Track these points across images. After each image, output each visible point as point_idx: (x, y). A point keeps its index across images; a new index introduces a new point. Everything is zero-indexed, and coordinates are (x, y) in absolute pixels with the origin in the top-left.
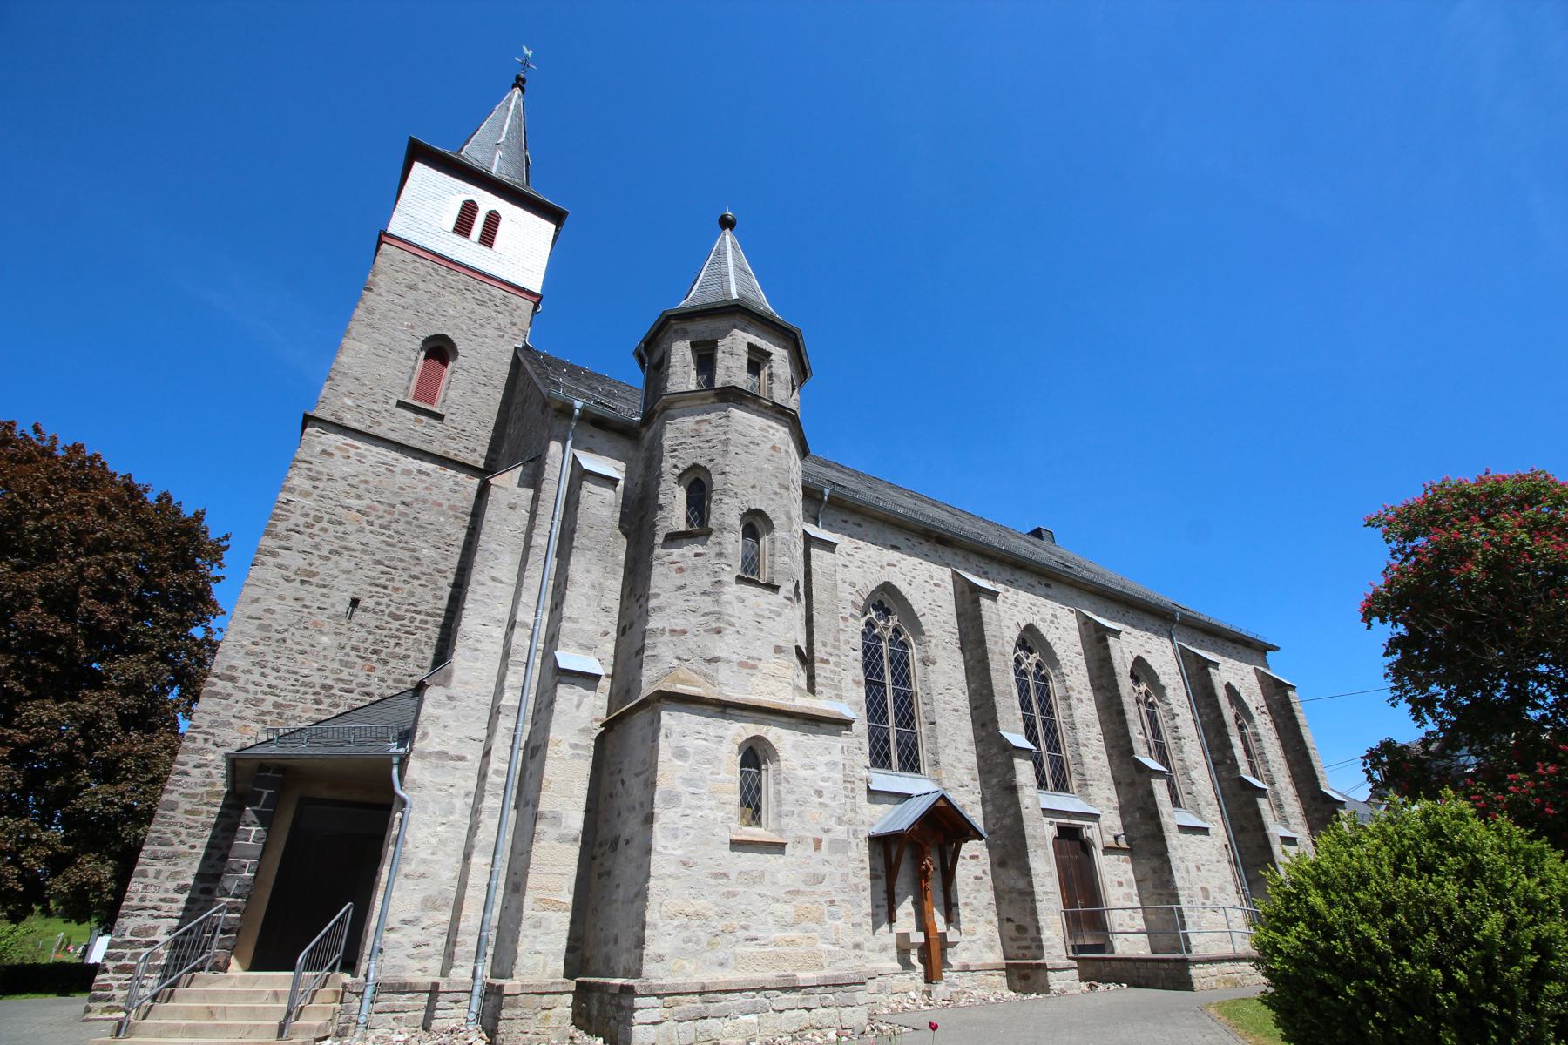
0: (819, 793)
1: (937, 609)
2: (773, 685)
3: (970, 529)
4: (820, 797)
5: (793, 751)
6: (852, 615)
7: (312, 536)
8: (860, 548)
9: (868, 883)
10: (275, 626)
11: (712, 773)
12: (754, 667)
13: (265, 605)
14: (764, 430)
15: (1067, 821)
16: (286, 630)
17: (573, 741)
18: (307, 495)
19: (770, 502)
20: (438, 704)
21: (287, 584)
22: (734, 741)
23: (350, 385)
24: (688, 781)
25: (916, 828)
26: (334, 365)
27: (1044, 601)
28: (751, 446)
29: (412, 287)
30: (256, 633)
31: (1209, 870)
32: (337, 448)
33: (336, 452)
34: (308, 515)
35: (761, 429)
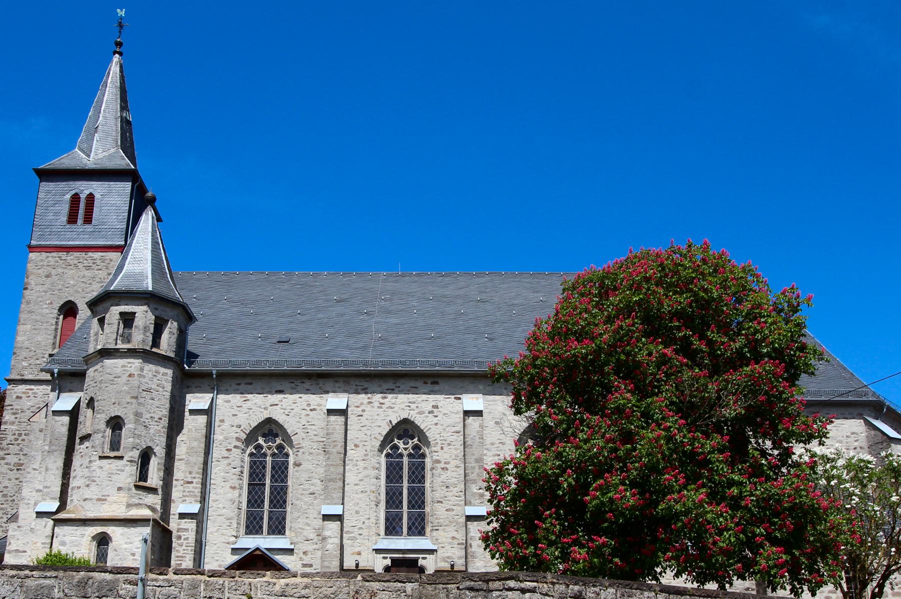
0: (133, 555)
1: (309, 427)
2: (114, 507)
4: (134, 556)
5: (121, 537)
6: (235, 447)
8: (248, 400)
10: (9, 494)
11: (77, 550)
15: (401, 556)
16: (14, 495)
17: (43, 542)
18: (13, 423)
19: (124, 409)
20: (14, 530)
21: (12, 472)
23: (24, 354)
26: (15, 345)
27: (424, 397)
28: (116, 379)
29: (48, 276)
32: (23, 393)
33: (23, 395)
34: (15, 434)
35: (123, 366)
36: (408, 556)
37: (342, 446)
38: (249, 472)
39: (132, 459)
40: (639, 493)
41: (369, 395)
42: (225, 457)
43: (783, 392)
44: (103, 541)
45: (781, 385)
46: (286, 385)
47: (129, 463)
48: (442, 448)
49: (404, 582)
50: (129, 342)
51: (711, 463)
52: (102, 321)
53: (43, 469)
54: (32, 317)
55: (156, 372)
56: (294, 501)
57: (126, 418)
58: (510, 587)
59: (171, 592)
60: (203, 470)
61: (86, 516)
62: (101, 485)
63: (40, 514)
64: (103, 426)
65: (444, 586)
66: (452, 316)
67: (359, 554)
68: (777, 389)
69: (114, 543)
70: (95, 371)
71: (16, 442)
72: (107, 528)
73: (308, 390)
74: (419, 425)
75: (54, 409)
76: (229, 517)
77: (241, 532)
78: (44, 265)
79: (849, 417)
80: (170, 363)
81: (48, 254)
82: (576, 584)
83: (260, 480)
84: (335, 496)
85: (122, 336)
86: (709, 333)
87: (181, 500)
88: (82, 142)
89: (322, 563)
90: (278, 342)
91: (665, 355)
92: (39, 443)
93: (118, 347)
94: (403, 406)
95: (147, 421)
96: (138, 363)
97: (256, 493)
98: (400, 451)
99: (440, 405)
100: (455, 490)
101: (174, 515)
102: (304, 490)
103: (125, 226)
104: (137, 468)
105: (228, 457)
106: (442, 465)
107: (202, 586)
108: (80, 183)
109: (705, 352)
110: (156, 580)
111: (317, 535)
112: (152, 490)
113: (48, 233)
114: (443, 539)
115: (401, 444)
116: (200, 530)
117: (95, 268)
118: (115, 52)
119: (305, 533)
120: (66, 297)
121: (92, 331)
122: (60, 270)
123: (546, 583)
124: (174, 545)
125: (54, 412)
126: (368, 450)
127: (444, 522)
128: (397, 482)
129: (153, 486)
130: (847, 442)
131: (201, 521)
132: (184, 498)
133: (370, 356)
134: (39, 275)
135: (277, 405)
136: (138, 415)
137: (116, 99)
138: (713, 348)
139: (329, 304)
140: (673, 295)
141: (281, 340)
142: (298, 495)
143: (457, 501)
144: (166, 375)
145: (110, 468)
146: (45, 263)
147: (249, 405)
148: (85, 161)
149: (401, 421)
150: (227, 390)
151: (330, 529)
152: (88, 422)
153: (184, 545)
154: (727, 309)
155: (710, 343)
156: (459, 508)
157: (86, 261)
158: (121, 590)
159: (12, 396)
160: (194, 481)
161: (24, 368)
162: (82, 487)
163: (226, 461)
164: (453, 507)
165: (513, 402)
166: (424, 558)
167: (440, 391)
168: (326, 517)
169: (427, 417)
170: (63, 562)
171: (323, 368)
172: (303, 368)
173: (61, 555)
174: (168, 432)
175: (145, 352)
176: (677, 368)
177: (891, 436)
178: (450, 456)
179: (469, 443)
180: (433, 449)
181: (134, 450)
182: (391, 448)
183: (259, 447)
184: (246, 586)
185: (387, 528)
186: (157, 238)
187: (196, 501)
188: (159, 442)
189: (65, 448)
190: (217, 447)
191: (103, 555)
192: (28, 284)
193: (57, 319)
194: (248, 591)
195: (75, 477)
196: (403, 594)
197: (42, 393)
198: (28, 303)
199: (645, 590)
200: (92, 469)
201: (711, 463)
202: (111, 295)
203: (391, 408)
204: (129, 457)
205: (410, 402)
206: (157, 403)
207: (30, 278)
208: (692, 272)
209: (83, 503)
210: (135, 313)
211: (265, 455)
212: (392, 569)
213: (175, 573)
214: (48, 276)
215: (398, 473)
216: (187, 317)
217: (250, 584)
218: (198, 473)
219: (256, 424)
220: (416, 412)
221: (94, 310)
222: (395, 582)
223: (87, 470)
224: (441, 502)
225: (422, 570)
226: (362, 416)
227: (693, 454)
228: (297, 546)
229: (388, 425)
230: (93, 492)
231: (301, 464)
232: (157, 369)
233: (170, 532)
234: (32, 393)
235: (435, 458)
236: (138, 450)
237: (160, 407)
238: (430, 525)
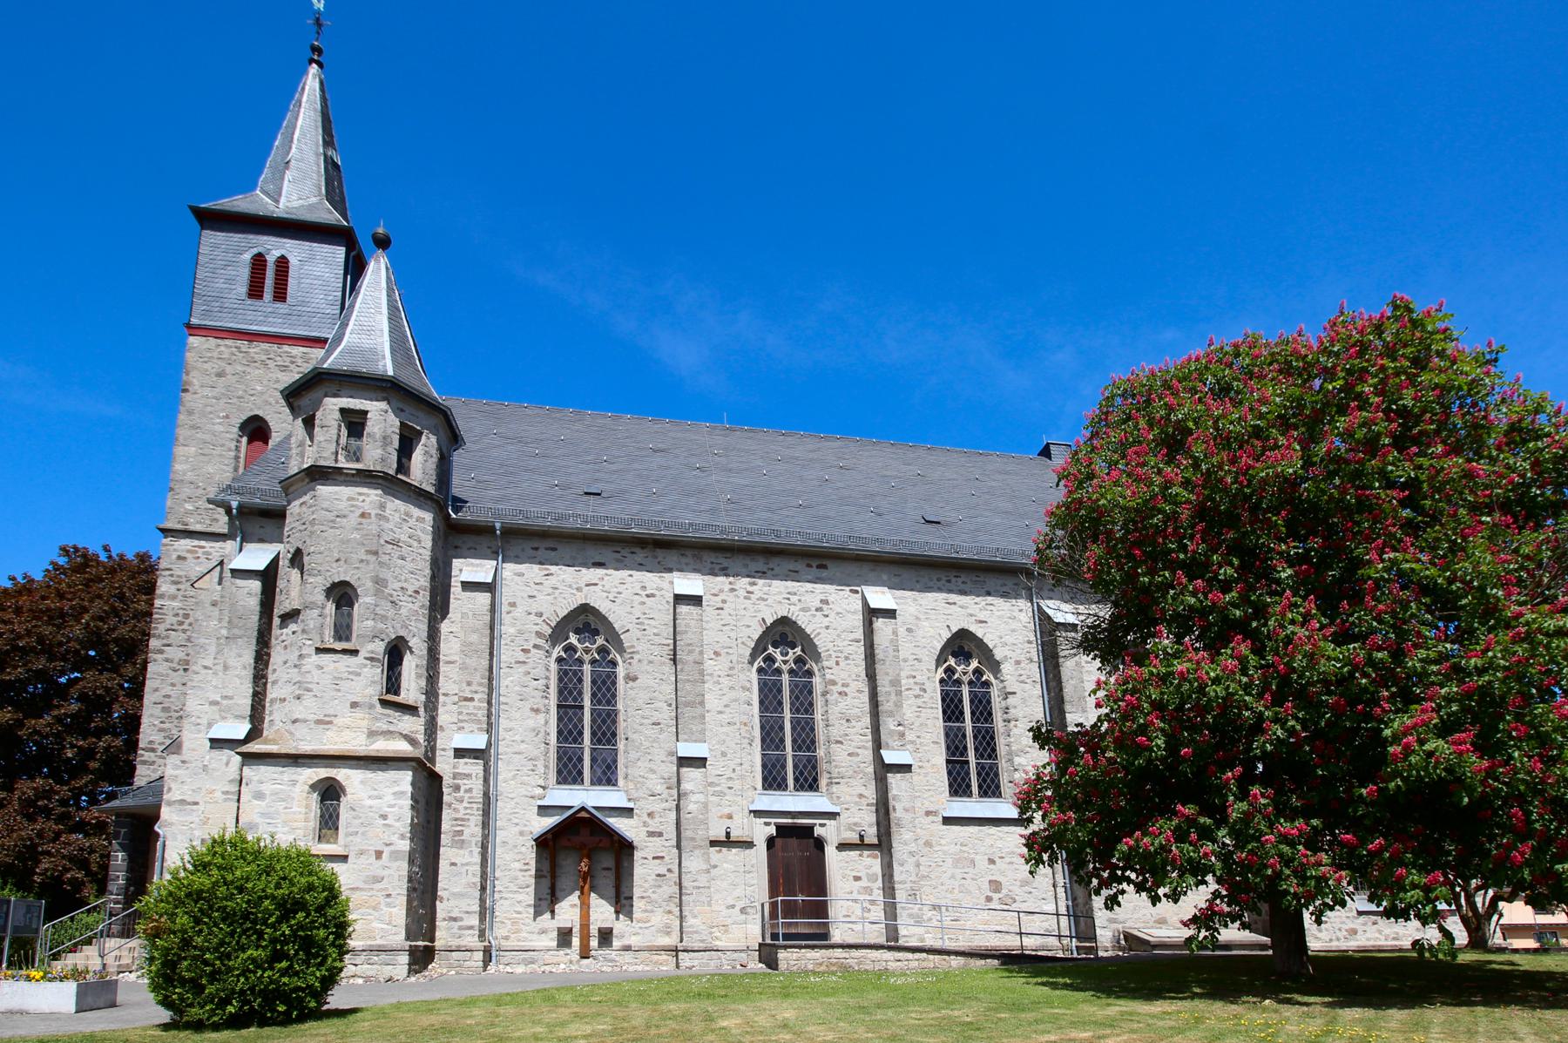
0: (384, 817)
1: (646, 622)
2: (347, 735)
3: (674, 532)
6: (535, 646)
7: (184, 631)
8: (552, 574)
9: (533, 881)
11: (286, 808)
13: (163, 692)
14: (353, 499)
15: (790, 821)
18: (173, 598)
20: (176, 767)
22: (305, 783)
23: (187, 491)
24: (263, 815)
25: (549, 836)
26: (172, 476)
27: (809, 586)
28: (338, 519)
29: (219, 375)
30: (162, 714)
31: (1010, 863)
32: (189, 551)
33: (188, 555)
34: (177, 615)
35: (350, 499)
36: (796, 821)
39: (373, 655)
41: (731, 579)
42: (520, 662)
44: (330, 792)
46: (606, 554)
47: (369, 662)
48: (837, 663)
50: (358, 460)
52: (309, 423)
53: (220, 668)
56: (630, 735)
57: (359, 587)
61: (298, 749)
62: (321, 697)
63: (217, 743)
64: (320, 597)
67: (730, 817)
69: (349, 796)
70: (302, 504)
71: (181, 628)
72: (335, 770)
73: (641, 564)
75: (233, 566)
76: (532, 756)
78: (212, 357)
80: (429, 502)
81: (219, 341)
83: (575, 700)
85: (346, 449)
87: (454, 727)
88: (265, 181)
92: (212, 625)
93: (340, 465)
94: (779, 598)
95: (395, 593)
96: (377, 495)
97: (570, 720)
98: (777, 665)
99: (831, 599)
101: (444, 750)
102: (643, 717)
103: (341, 285)
104: (383, 670)
105: (524, 662)
106: (839, 688)
108: (265, 238)
111: (668, 788)
112: (410, 709)
113: (216, 309)
118: (312, 61)
119: (649, 784)
120: (251, 410)
122: (239, 368)
124: (446, 798)
125: (233, 571)
128: (775, 710)
129: (411, 702)
132: (462, 725)
133: (724, 521)
134: (205, 373)
135: (596, 584)
136: (379, 582)
139: (644, 453)
142: (636, 726)
143: (862, 741)
145: (336, 669)
146: (215, 354)
147: (554, 582)
148: (272, 208)
150: (517, 557)
152: (291, 591)
153: (466, 800)
159: (170, 556)
160: (476, 697)
161: (187, 512)
162: (288, 699)
163: (522, 669)
166: (822, 825)
169: (814, 616)
170: (250, 858)
178: (850, 676)
180: (825, 664)
182: (765, 660)
183: (570, 649)
185: (765, 779)
186: (396, 301)
187: (480, 729)
188: (416, 630)
189: (256, 633)
190: (506, 645)
191: (331, 816)
192: (187, 383)
193: (238, 441)
195: (274, 683)
197: (219, 554)
198: (190, 413)
200: (304, 669)
204: (368, 652)
205: (789, 593)
207: (192, 374)
209: (292, 728)
211: (580, 662)
212: (779, 842)
214: (219, 375)
216: (452, 438)
218: (480, 684)
219: (566, 612)
220: (798, 608)
221: (295, 404)
223: (296, 670)
224: (841, 743)
229: (761, 626)
230: (307, 709)
235: (828, 676)
236: (383, 640)
237: (414, 571)
238: (825, 775)
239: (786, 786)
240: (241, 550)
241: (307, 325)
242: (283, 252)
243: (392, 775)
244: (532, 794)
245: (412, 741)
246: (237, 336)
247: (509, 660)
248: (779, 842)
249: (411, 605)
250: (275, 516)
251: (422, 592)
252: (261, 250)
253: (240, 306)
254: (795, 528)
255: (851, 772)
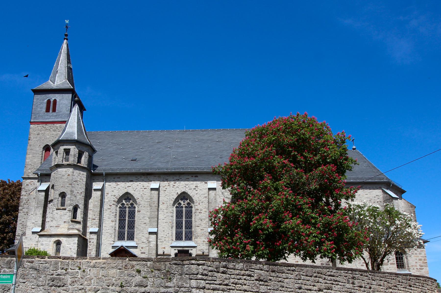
0: (71, 249)
1: (144, 196)
6: (113, 204)
12: (59, 227)
15: (182, 249)
18: (25, 196)
19: (66, 189)
20: (24, 239)
22: (53, 241)
25: (113, 254)
26: (25, 163)
27: (192, 182)
29: (38, 134)
32: (29, 183)
34: (26, 200)
36: (184, 249)
37: (157, 203)
38: (119, 214)
40: (273, 222)
41: (169, 182)
42: (109, 209)
43: (335, 178)
44: (58, 243)
45: (335, 175)
46: (133, 178)
47: (68, 211)
48: (199, 204)
49: (147, 261)
50: (68, 161)
51: (303, 209)
52: (57, 153)
53: (35, 214)
54: (32, 152)
55: (79, 174)
56: (137, 227)
58: (192, 263)
59: (46, 266)
60: (100, 214)
63: (34, 233)
65: (164, 263)
66: (205, 148)
67: (164, 248)
68: (333, 177)
72: (60, 238)
73: (143, 180)
74: (189, 194)
77: (116, 239)
79: (375, 188)
80: (85, 170)
82: (224, 262)
83: (124, 218)
84: (154, 224)
85: (65, 159)
86: (304, 153)
89: (149, 251)
90: (132, 160)
91: (284, 163)
92: (33, 204)
95: (76, 194)
96: (72, 170)
97: (122, 223)
98: (182, 205)
100: (204, 222)
101: (88, 232)
102: (141, 222)
105: (110, 209)
106: (199, 211)
107: (60, 263)
108: (51, 95)
109: (303, 161)
110: (40, 261)
112: (79, 223)
114: (199, 242)
115: (182, 202)
116: (99, 239)
117: (58, 131)
118: (65, 39)
119: (142, 240)
121: (53, 157)
122: (43, 132)
123: (210, 261)
124: (88, 245)
125: (38, 190)
126: (168, 205)
127: (200, 235)
129: (79, 221)
130: (374, 200)
131: (99, 235)
132: (92, 226)
135: (130, 187)
136: (72, 191)
137: (65, 59)
138: (307, 160)
140: (289, 136)
141: (133, 159)
142: (139, 224)
143: (205, 226)
144: (83, 175)
146: (37, 129)
149: (182, 193)
150: (109, 181)
151: (152, 238)
152: (53, 194)
153: (92, 245)
154: (313, 142)
155: (305, 157)
156: (206, 229)
157: (53, 128)
158: (25, 265)
159: (25, 184)
160: (96, 218)
161: (29, 173)
163: (109, 210)
164: (204, 228)
165: (222, 184)
167: (198, 180)
168: (150, 233)
169: (193, 191)
171: (149, 171)
172: (141, 171)
173: (35, 249)
174: (85, 199)
175: (74, 165)
176: (290, 168)
177: (393, 197)
178: (203, 207)
179: (210, 201)
180: (196, 204)
181: (71, 206)
182: (122, 205)
183: (123, 204)
184: (78, 263)
185: (176, 237)
186: (80, 117)
187: (97, 227)
191: (58, 249)
192: (30, 138)
193: (42, 152)
194: (79, 265)
196: (146, 266)
198: (30, 146)
199: (258, 264)
200: (53, 214)
201: (303, 209)
202: (60, 141)
203: (178, 187)
205: (186, 185)
206: (80, 186)
208: (298, 127)
209: (50, 228)
210: (70, 149)
211: (126, 207)
212: (179, 255)
213: (48, 258)
214: (38, 134)
215: (181, 214)
217: (80, 262)
218: (97, 215)
219: (122, 195)
220: (188, 189)
222: (143, 261)
224: (199, 226)
225: (191, 255)
226: (166, 191)
227: (295, 206)
228: (139, 245)
229: (177, 194)
230: (54, 223)
231: (140, 211)
232: (80, 172)
233: (87, 240)
234: (33, 183)
235: (196, 208)
237: (81, 188)
238: (194, 236)
239: (183, 239)
240: (41, 185)
241: (61, 118)
242: (55, 98)
243: (73, 239)
244: (111, 243)
245: (78, 230)
246: (43, 123)
247: (106, 208)
248: (179, 255)
249: (80, 196)
250: (49, 175)
251: (83, 193)
252: (49, 98)
253: (44, 115)
254: (191, 167)
255: (201, 235)
